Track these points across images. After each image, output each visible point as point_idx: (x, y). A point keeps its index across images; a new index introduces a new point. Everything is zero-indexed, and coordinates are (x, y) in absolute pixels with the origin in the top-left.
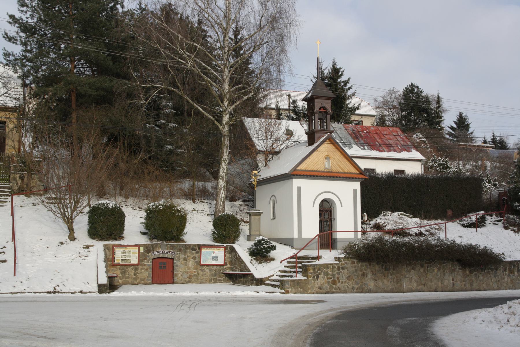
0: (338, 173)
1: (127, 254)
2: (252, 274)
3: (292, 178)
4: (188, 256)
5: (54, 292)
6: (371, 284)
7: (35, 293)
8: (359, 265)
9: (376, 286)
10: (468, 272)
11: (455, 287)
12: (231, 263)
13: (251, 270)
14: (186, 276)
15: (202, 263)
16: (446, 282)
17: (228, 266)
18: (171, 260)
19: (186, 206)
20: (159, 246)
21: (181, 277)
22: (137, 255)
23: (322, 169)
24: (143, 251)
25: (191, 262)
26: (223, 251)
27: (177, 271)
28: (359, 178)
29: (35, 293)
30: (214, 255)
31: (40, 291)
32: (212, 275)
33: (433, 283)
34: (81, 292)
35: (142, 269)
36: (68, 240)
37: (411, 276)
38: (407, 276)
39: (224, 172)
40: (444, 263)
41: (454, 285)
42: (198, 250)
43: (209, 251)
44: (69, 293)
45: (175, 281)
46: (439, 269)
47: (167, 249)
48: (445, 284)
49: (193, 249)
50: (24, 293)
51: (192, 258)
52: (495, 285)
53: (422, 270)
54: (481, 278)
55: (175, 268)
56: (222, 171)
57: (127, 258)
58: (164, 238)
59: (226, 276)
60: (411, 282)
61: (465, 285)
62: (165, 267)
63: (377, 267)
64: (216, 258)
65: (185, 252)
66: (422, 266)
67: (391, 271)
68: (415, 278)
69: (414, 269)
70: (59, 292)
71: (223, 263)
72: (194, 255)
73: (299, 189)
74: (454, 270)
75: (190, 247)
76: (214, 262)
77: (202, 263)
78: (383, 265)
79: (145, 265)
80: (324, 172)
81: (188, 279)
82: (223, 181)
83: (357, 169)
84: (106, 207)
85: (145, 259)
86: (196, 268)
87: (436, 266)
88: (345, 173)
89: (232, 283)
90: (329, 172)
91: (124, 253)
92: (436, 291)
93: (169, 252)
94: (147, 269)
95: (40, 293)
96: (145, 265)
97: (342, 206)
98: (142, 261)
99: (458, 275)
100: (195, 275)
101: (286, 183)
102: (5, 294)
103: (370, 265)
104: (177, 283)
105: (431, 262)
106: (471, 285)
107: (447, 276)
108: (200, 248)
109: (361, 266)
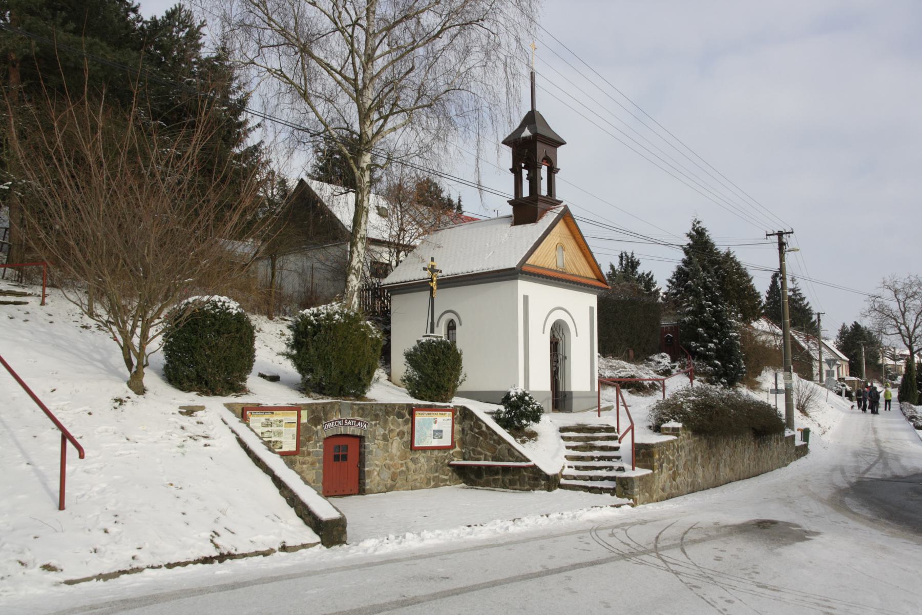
0: (573, 275)
1: (274, 428)
2: (535, 467)
3: (517, 279)
4: (391, 431)
5: (222, 558)
7: (170, 566)
12: (463, 443)
13: (529, 457)
14: (386, 475)
15: (416, 445)
17: (458, 449)
18: (358, 440)
19: (258, 321)
20: (336, 407)
21: (378, 478)
22: (294, 429)
23: (553, 267)
24: (305, 421)
25: (395, 445)
26: (450, 418)
27: (371, 465)
28: (595, 287)
29: (170, 566)
30: (435, 427)
31: (183, 560)
32: (430, 470)
34: (284, 548)
35: (304, 463)
36: (131, 393)
39: (360, 261)
42: (407, 416)
43: (427, 417)
44: (257, 553)
45: (367, 487)
47: (353, 416)
49: (400, 415)
50: (138, 570)
51: (398, 435)
55: (368, 457)
56: (357, 260)
57: (273, 439)
58: (340, 392)
59: (454, 471)
62: (345, 458)
64: (438, 434)
65: (386, 421)
70: (231, 556)
71: (449, 444)
72: (401, 428)
73: (526, 298)
75: (394, 410)
76: (435, 443)
77: (416, 445)
79: (309, 454)
80: (556, 271)
81: (390, 482)
82: (357, 278)
83: (594, 272)
84: (225, 312)
85: (309, 440)
86: (403, 457)
88: (581, 276)
89: (463, 485)
90: (563, 272)
91: (267, 425)
93: (357, 422)
94: (313, 464)
95: (185, 564)
96: (309, 454)
98: (305, 445)
100: (402, 472)
101: (502, 287)
102: (83, 584)
104: (371, 492)
108: (412, 414)
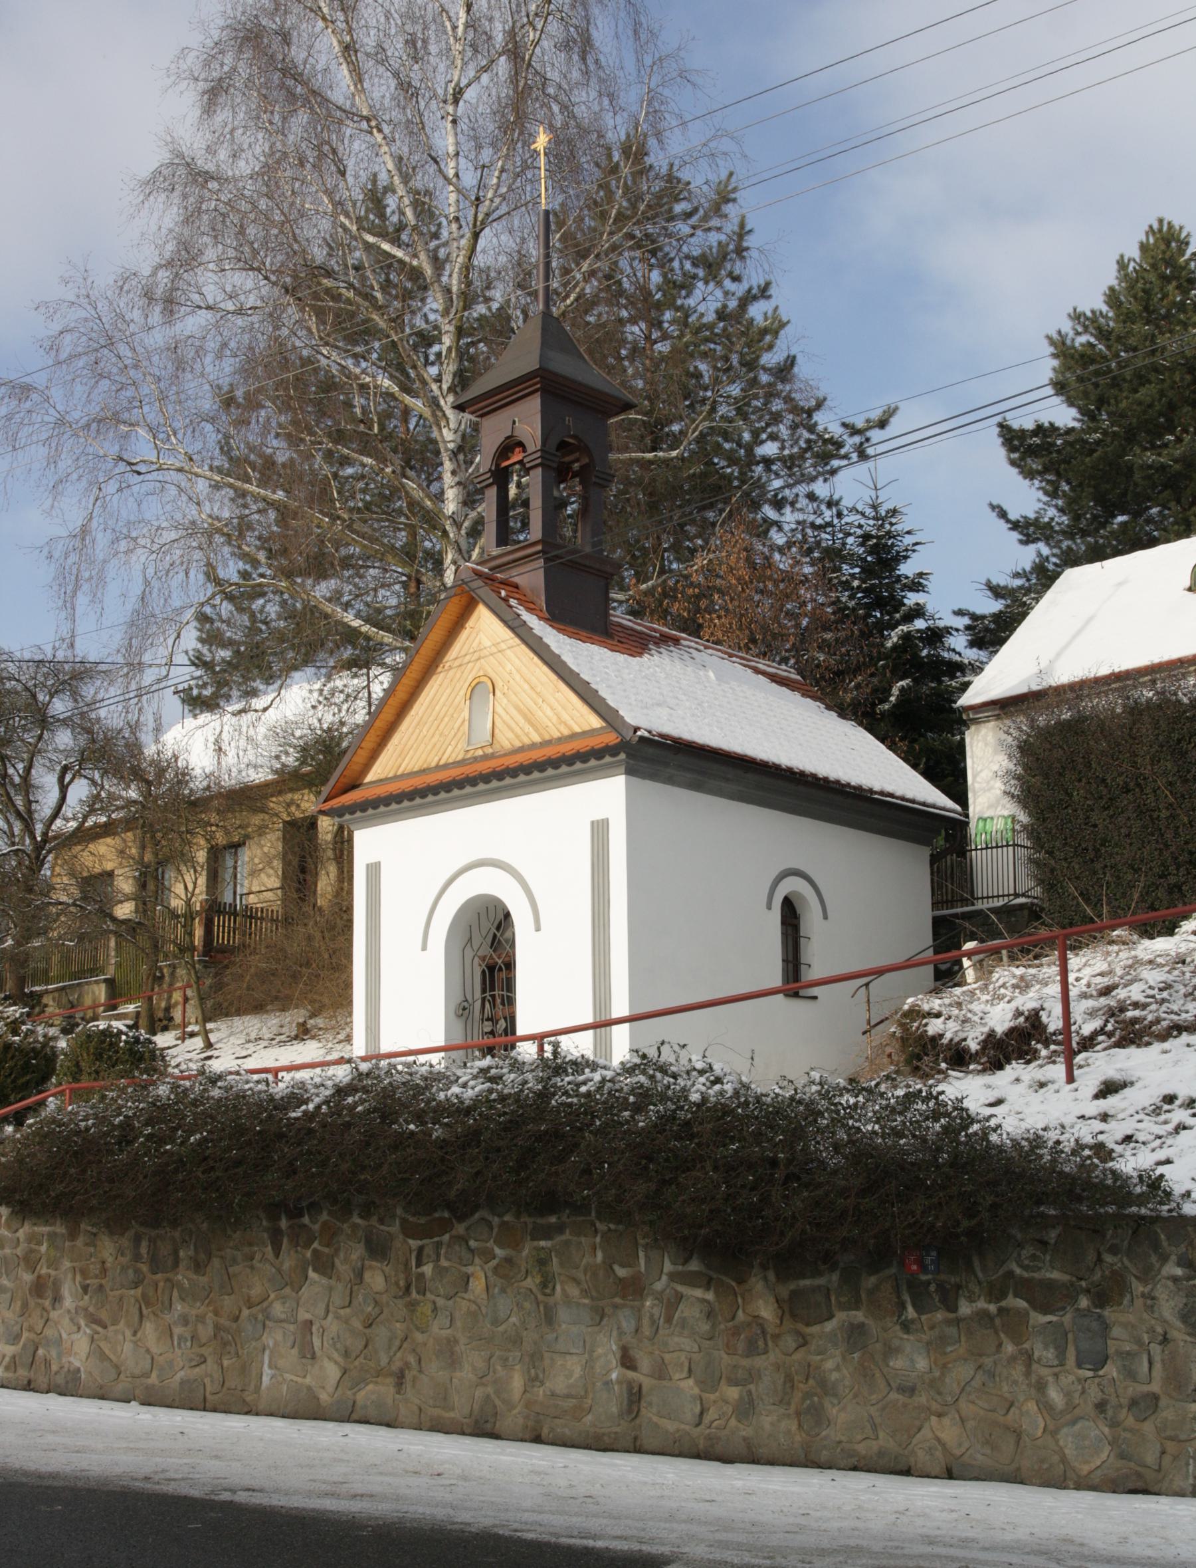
0: (522, 749)
6: (77, 1348)
8: (21, 1234)
9: (103, 1357)
10: (766, 1310)
11: (649, 1414)
16: (566, 1373)
33: (465, 1374)
37: (307, 1309)
38: (278, 1309)
40: (547, 1233)
41: (635, 1396)
46: (506, 1271)
48: (558, 1383)
52: (1088, 1443)
53: (376, 1279)
54: (913, 1360)
60: (309, 1354)
61: (745, 1410)
63: (107, 1248)
66: (377, 1249)
67: (183, 1276)
68: (331, 1330)
69: (325, 1266)
74: (634, 1289)
78: (137, 1240)
87: (488, 1255)
92: (483, 1427)
97: (538, 929)
99: (679, 1325)
103: (73, 1235)
105: (445, 1226)
106: (812, 1415)
107: (571, 1324)
109: (31, 1238)
